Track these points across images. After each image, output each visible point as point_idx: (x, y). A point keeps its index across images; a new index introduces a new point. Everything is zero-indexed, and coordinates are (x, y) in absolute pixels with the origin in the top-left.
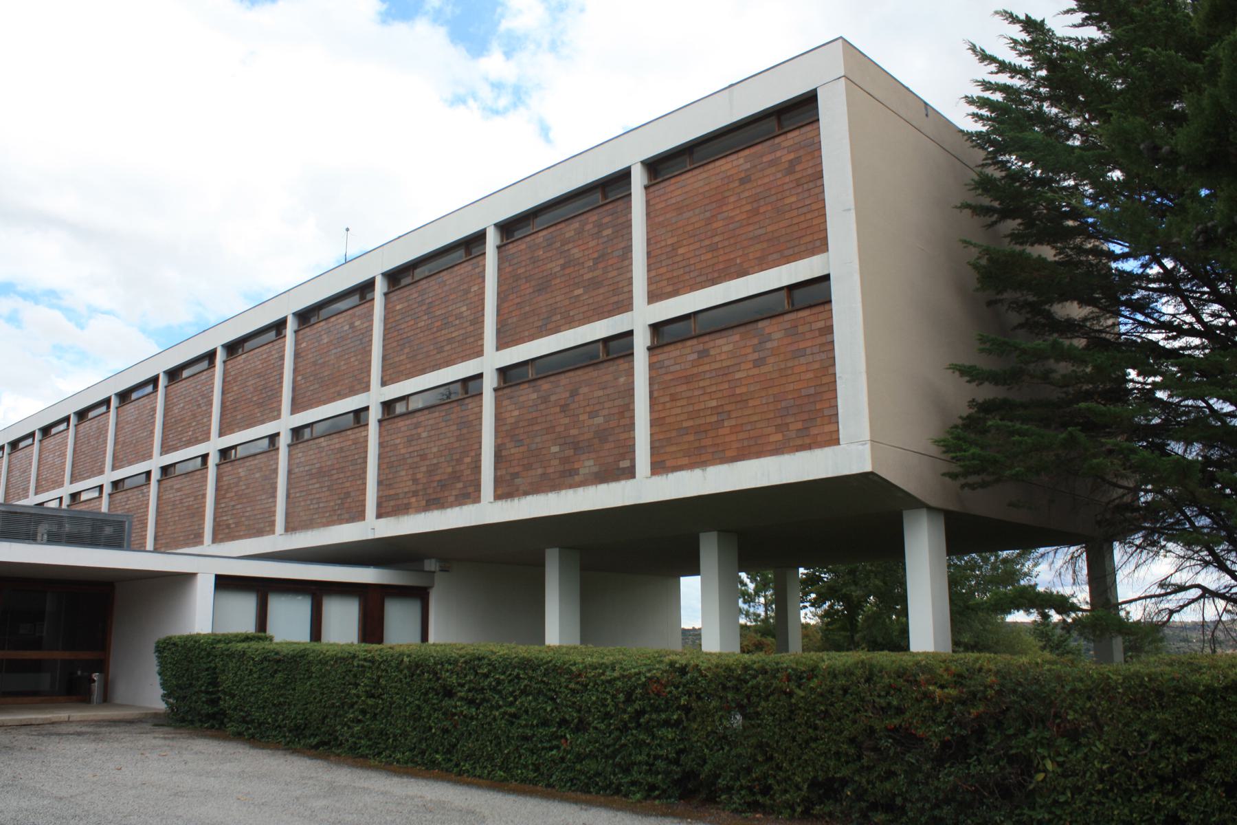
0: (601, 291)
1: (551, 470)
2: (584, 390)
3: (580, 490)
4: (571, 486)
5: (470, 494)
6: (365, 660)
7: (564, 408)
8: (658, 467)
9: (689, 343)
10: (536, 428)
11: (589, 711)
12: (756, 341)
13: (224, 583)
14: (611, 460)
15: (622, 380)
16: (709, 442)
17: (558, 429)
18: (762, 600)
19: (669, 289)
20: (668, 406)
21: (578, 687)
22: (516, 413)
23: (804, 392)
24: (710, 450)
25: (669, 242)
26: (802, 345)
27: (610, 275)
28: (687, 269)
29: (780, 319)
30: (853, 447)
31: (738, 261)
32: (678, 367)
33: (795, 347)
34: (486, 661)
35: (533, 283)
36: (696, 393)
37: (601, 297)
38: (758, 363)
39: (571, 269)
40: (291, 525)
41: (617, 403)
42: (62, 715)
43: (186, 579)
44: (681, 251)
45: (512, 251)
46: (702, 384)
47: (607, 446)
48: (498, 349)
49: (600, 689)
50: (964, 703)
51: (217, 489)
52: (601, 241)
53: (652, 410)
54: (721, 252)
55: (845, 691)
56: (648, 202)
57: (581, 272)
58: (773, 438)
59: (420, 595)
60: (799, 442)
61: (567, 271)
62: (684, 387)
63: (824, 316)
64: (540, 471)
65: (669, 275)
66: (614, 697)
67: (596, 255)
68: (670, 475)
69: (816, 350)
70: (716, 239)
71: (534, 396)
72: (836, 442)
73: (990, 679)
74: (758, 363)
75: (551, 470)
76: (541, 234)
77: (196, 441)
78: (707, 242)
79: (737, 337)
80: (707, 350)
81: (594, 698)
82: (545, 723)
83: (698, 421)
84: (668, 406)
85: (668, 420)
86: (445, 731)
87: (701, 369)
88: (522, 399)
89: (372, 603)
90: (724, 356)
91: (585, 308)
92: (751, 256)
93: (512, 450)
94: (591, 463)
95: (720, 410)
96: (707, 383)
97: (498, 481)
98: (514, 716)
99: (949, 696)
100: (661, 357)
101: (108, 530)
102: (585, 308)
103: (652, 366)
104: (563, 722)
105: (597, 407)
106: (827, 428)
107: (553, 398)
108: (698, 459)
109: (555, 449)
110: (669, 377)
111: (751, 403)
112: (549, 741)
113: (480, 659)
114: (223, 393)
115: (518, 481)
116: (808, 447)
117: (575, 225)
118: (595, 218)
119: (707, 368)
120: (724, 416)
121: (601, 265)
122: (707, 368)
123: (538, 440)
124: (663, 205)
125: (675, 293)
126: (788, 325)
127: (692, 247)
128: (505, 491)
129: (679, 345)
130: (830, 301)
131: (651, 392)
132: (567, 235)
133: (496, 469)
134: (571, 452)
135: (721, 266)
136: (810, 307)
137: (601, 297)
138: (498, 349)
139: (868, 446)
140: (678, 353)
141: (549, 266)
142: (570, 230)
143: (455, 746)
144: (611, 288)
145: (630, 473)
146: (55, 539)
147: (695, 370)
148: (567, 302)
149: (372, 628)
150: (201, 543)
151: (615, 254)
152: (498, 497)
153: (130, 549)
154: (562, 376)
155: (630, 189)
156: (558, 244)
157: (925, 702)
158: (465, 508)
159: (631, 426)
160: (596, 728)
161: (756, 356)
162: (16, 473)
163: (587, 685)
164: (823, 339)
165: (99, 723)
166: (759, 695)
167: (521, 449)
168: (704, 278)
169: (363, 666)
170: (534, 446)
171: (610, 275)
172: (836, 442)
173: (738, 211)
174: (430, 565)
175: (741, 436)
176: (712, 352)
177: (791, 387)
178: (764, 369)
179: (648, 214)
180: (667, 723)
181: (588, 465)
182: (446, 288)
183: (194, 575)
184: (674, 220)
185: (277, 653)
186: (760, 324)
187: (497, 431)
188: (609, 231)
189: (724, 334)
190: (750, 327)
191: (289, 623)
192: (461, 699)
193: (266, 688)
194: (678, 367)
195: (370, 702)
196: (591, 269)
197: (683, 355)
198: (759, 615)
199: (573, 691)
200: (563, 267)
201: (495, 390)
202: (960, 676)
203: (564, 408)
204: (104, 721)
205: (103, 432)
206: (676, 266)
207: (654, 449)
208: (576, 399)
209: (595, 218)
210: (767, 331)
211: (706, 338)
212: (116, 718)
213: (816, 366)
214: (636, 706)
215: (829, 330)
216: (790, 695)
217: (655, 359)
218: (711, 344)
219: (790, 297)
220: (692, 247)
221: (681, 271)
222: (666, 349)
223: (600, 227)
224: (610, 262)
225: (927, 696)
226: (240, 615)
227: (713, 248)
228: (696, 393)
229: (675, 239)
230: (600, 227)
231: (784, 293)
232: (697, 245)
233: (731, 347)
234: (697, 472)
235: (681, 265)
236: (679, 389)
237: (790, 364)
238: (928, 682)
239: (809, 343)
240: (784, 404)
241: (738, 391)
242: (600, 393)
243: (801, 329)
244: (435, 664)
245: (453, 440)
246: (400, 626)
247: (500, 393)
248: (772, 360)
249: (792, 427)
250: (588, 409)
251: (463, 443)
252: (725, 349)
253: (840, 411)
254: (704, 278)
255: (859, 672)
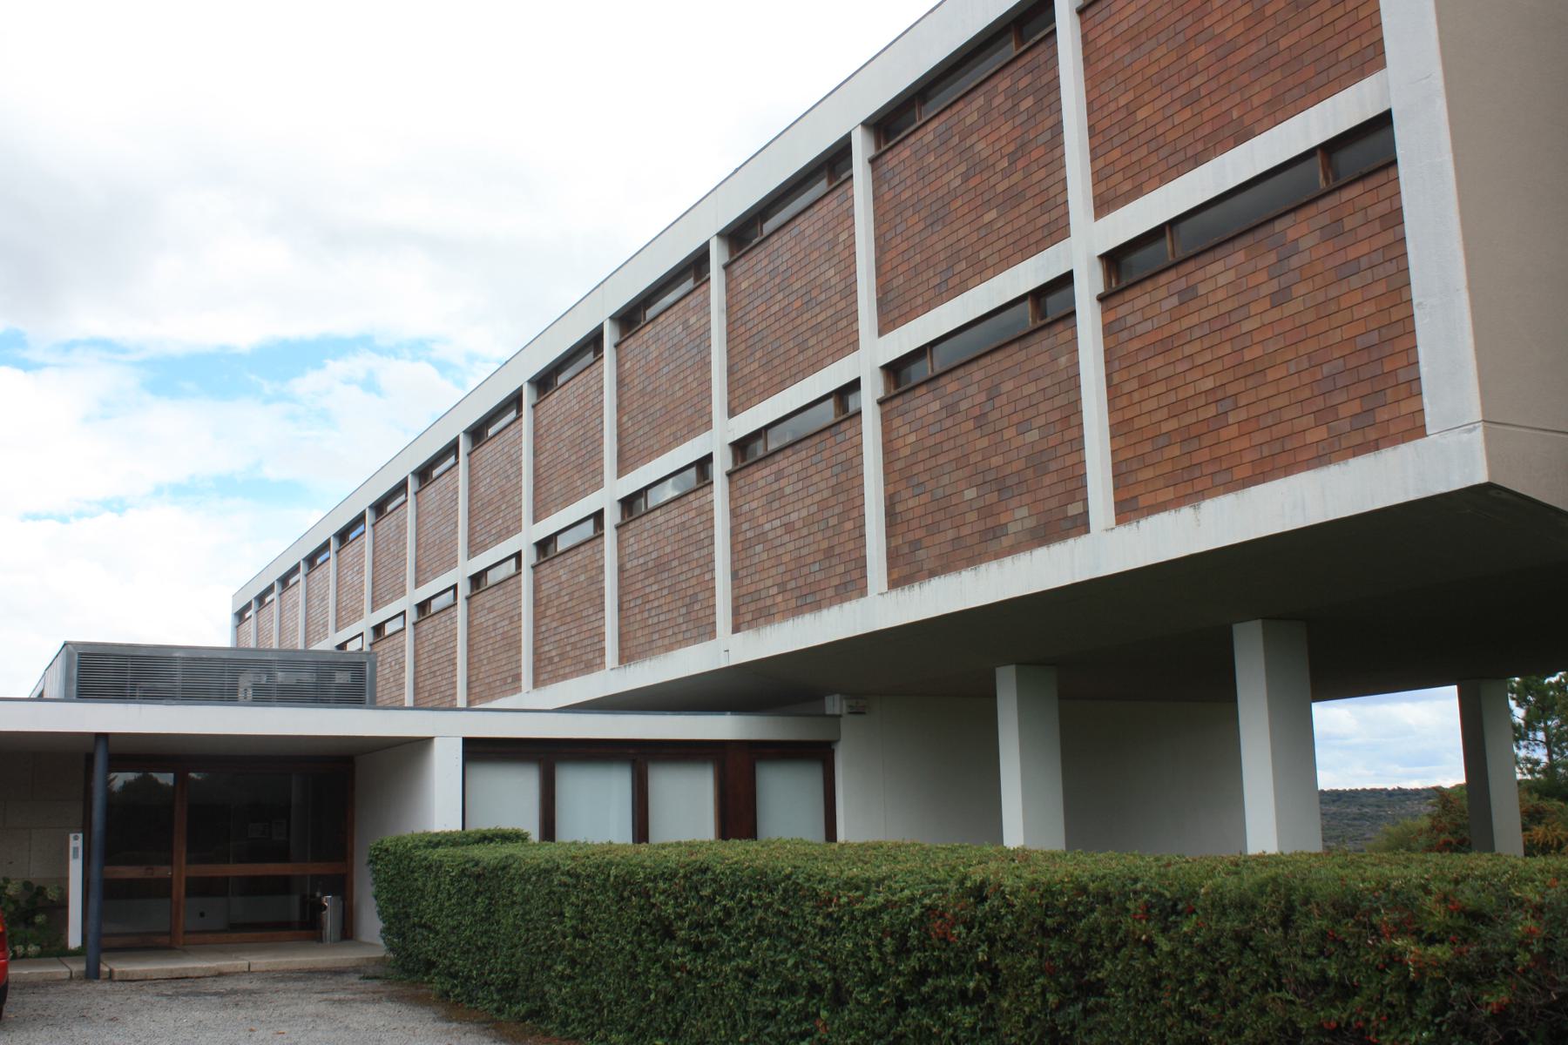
0: (1024, 208)
1: (966, 531)
2: (1008, 386)
3: (1008, 561)
4: (998, 556)
5: (852, 586)
6: (568, 873)
7: (980, 420)
8: (1128, 509)
9: (1164, 279)
10: (942, 459)
11: (846, 970)
12: (1272, 258)
13: (478, 751)
14: (1053, 503)
15: (1063, 360)
16: (1204, 455)
17: (973, 459)
18: (1541, 736)
19: (1127, 186)
20: (1136, 397)
21: (828, 923)
22: (912, 438)
23: (1361, 342)
24: (1208, 470)
25: (1122, 102)
26: (1352, 253)
27: (1036, 178)
28: (1153, 145)
29: (1311, 211)
30: (1451, 437)
31: (1235, 115)
32: (1148, 325)
33: (1340, 258)
34: (709, 875)
35: (923, 214)
36: (1180, 368)
37: (1023, 220)
38: (1280, 298)
39: (977, 180)
40: (627, 653)
41: (1058, 402)
42: (240, 962)
43: (418, 747)
44: (1141, 115)
45: (891, 164)
46: (1188, 350)
47: (1047, 480)
48: (881, 333)
49: (860, 928)
50: (1466, 977)
51: (537, 603)
52: (1018, 121)
53: (1112, 409)
54: (1206, 103)
55: (1243, 940)
56: (1084, 37)
57: (992, 181)
58: (1311, 437)
59: (818, 754)
60: (1357, 438)
61: (972, 184)
62: (1160, 361)
63: (1386, 192)
64: (951, 534)
65: (1125, 161)
66: (879, 944)
67: (1011, 148)
68: (1143, 523)
69: (1377, 258)
70: (1196, 82)
71: (935, 406)
72: (1419, 431)
73: (1524, 924)
74: (1280, 298)
75: (966, 531)
76: (930, 127)
77: (502, 536)
78: (1182, 90)
79: (1240, 257)
80: (1193, 288)
81: (849, 945)
82: (790, 989)
83: (1189, 419)
84: (1136, 397)
85: (1137, 424)
86: (669, 1000)
87: (1186, 323)
88: (919, 413)
89: (736, 771)
90: (1220, 295)
91: (1001, 243)
92: (1256, 102)
93: (910, 503)
94: (1024, 512)
95: (1220, 395)
96: (1197, 346)
97: (893, 557)
98: (752, 974)
99: (1437, 964)
100: (1122, 311)
101: (342, 678)
102: (1001, 243)
103: (1109, 330)
104: (815, 989)
105: (1029, 413)
106: (1405, 407)
107: (963, 406)
108: (1189, 486)
109: (970, 494)
110: (1136, 345)
111: (1271, 375)
112: (798, 1022)
113: (704, 871)
114: (535, 455)
115: (921, 554)
116: (1373, 446)
117: (979, 100)
118: (1007, 83)
119: (1194, 319)
120: (1228, 404)
121: (1020, 164)
122: (1194, 319)
123: (945, 480)
124: (1108, 37)
125: (1137, 192)
126: (1325, 220)
127: (1159, 104)
128: (903, 574)
129: (1148, 285)
130: (1394, 162)
131: (1109, 376)
132: (968, 121)
133: (889, 536)
134: (994, 497)
135: (1207, 129)
136: (1362, 177)
137: (1023, 220)
138: (881, 333)
139: (1479, 435)
140: (1147, 299)
141: (946, 179)
142: (970, 112)
143: (679, 1025)
144: (1038, 200)
145: (1080, 525)
146: (263, 696)
147: (1176, 327)
148: (974, 237)
149: (737, 814)
150: (517, 689)
151: (1042, 139)
152: (895, 583)
153: (374, 705)
154: (974, 367)
155: (1053, 20)
156: (956, 140)
157: (1390, 977)
158: (846, 605)
159: (1078, 444)
160: (858, 1002)
161: (1274, 286)
162: (315, 602)
163: (840, 919)
164: (1389, 237)
165: (311, 973)
166: (1101, 947)
167: (925, 498)
168: (1181, 156)
169: (565, 885)
170: (939, 493)
171: (1036, 178)
172: (1419, 431)
173: (1229, 23)
174: (834, 705)
175: (1259, 438)
176: (1202, 290)
177: (1337, 336)
178: (1290, 308)
179: (1086, 59)
180: (964, 997)
181: (1020, 517)
182: (805, 243)
183: (430, 739)
184: (1127, 61)
185: (477, 864)
186: (1279, 225)
187: (887, 473)
188: (1029, 102)
189: (1220, 252)
190: (1261, 234)
191: (596, 811)
192: (685, 942)
193: (467, 921)
194: (1148, 325)
195: (578, 944)
196: (1006, 174)
197: (1154, 301)
198: (1537, 762)
199: (823, 931)
200: (966, 178)
201: (881, 402)
202: (1477, 916)
203: (980, 420)
204: (300, 971)
205: (401, 528)
206: (1135, 143)
207: (1120, 476)
208: (997, 402)
209: (1007, 83)
210: (1292, 234)
211: (1191, 266)
212: (321, 966)
213: (1380, 289)
214: (913, 962)
215: (1394, 218)
216: (1150, 946)
217: (1111, 317)
218: (1199, 275)
219: (1328, 166)
220: (1159, 104)
221: (1144, 151)
222: (1128, 295)
223: (1015, 96)
224: (1034, 155)
225: (1394, 959)
226: (511, 799)
227: (1192, 99)
228: (1180, 368)
229: (1131, 95)
230: (1015, 96)
231: (1318, 160)
232: (1166, 100)
233: (1230, 276)
234: (1186, 512)
235: (1143, 139)
236: (1152, 365)
237: (1333, 292)
238: (1399, 929)
239: (1364, 248)
240: (1326, 369)
241: (1248, 355)
242: (1032, 388)
243: (1349, 223)
244: (647, 879)
245: (826, 494)
246: (785, 803)
247: (888, 407)
248: (1301, 289)
249: (1344, 411)
250: (1015, 419)
251: (842, 498)
252: (1222, 280)
253: (1424, 369)
254: (1181, 156)
255: (1266, 903)
